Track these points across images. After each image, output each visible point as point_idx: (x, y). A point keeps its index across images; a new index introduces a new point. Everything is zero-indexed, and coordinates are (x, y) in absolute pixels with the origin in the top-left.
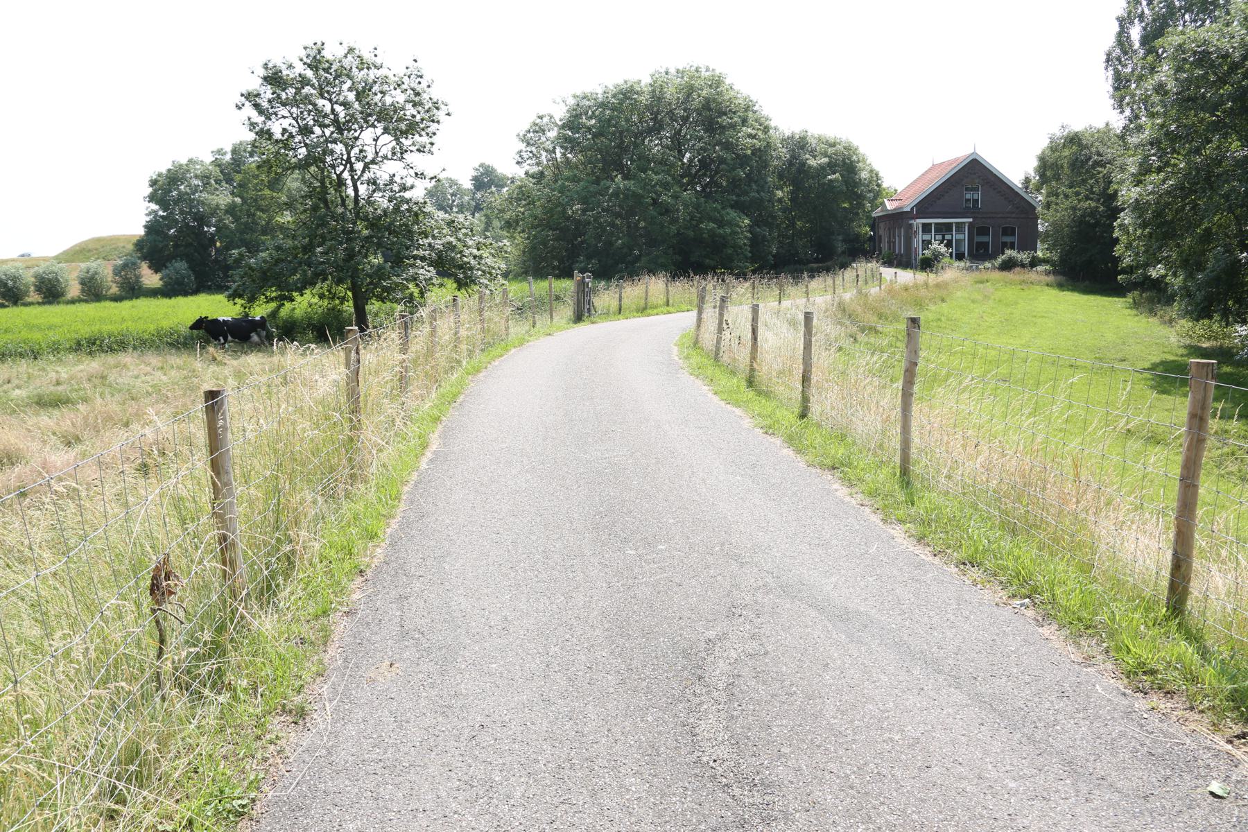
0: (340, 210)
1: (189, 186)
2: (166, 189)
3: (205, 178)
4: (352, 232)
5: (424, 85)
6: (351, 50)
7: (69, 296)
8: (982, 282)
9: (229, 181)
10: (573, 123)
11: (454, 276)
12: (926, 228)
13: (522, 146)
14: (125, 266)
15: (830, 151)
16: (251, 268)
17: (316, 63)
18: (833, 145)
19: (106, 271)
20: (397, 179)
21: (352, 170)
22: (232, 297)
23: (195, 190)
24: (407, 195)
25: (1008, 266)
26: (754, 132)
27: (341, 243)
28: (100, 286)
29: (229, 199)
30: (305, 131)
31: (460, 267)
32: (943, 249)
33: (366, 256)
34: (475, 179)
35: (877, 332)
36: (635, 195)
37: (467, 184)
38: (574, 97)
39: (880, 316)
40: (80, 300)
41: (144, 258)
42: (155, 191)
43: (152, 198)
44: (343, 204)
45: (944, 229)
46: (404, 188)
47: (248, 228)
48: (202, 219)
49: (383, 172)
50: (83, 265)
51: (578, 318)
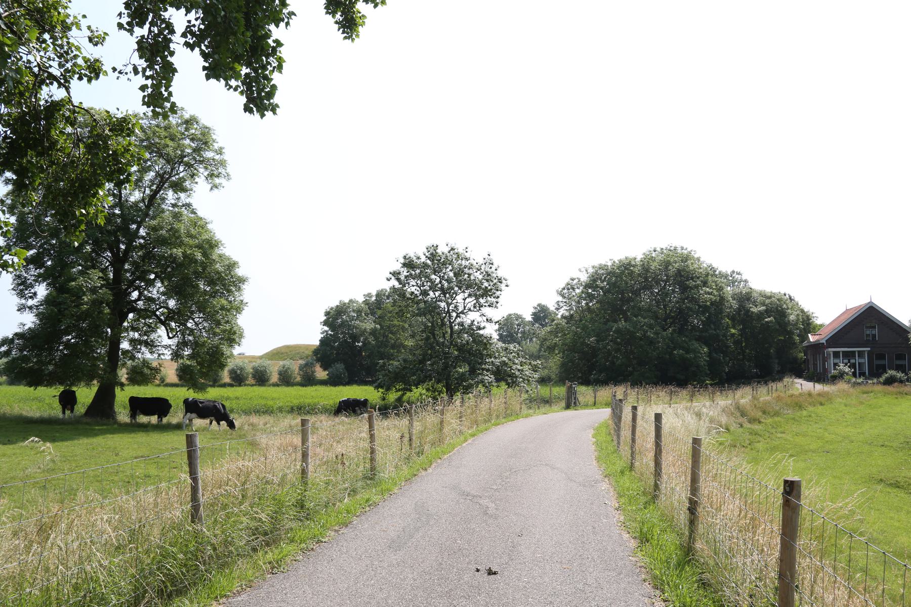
0: (441, 340)
1: (349, 316)
2: (336, 318)
3: (359, 312)
4: (448, 353)
5: (493, 269)
6: (452, 249)
7: (271, 382)
8: (867, 393)
9: (373, 314)
10: (592, 283)
11: (506, 381)
12: (836, 355)
13: (560, 299)
14: (306, 365)
15: (767, 301)
16: (389, 371)
17: (433, 256)
18: (770, 297)
19: (295, 367)
20: (476, 323)
21: (450, 316)
22: (377, 388)
23: (352, 318)
24: (481, 332)
25: (890, 381)
26: (711, 291)
27: (441, 360)
28: (290, 377)
29: (373, 326)
30: (425, 293)
31: (510, 376)
32: (847, 369)
33: (455, 368)
34: (534, 314)
35: (760, 422)
36: (629, 331)
37: (529, 318)
38: (593, 267)
39: (764, 412)
40: (278, 385)
41: (318, 360)
42: (328, 319)
43: (325, 323)
44: (444, 337)
45: (848, 355)
46: (479, 328)
47: (384, 344)
48: (355, 338)
49: (468, 319)
50: (281, 363)
51: (568, 407)
